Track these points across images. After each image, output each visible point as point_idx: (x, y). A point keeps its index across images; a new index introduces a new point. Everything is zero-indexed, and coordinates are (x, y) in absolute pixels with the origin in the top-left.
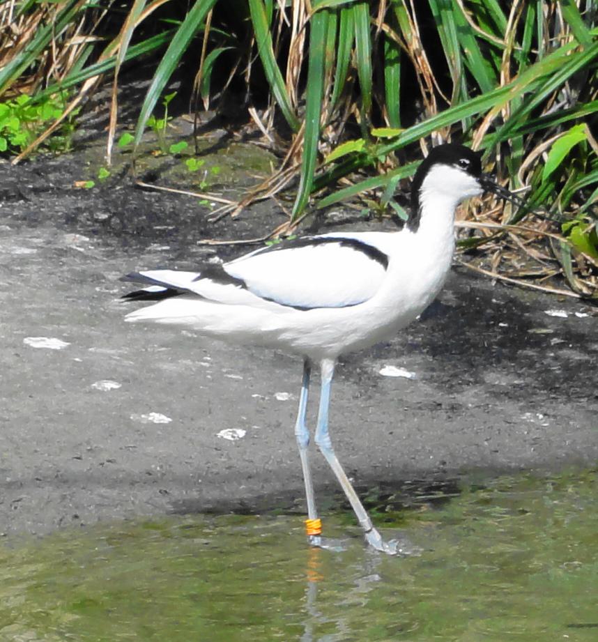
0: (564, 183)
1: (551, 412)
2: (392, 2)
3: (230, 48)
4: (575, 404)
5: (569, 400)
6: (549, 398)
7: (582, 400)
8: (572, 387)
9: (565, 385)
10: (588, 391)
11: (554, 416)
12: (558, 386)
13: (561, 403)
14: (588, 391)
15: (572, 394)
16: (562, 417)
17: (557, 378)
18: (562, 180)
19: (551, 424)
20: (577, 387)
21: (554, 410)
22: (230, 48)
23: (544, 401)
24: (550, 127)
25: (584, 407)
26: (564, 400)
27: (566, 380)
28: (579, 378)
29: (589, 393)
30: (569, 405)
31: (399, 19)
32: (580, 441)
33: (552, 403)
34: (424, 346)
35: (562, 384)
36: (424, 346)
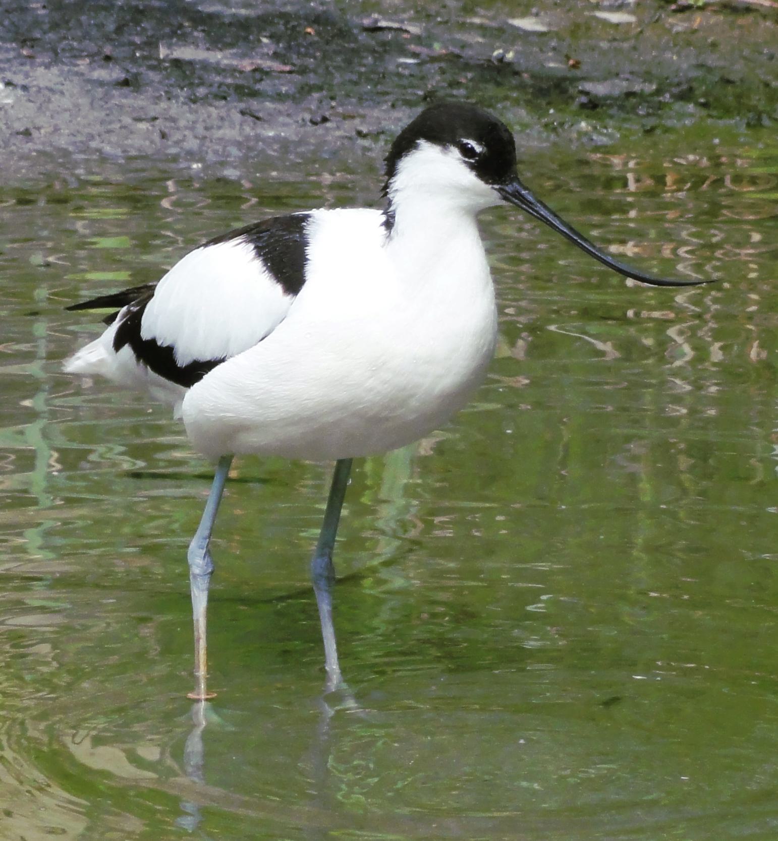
0: (37, 151)
1: (19, 79)
2: (47, 330)
3: (430, 518)
4: (66, 68)
5: (56, 59)
6: (20, 56)
7: (79, 62)
8: (65, 38)
9: (51, 36)
10: (92, 47)
11: (25, 88)
12: (38, 36)
13: (40, 66)
14: (92, 47)
15: (63, 50)
16: (39, 90)
17: (37, 23)
18: (35, 154)
19: (18, 100)
20: (73, 39)
21: (27, 75)
22: (430, 518)
23: (8, 60)
24: (13, 540)
25: (82, 74)
26: (47, 61)
27: (55, 26)
28: (80, 24)
29: (95, 49)
30: (55, 70)
31: (205, 609)
32: (67, 131)
33: (22, 64)
34: (38, 302)
35: (45, 33)
36: (38, 302)
